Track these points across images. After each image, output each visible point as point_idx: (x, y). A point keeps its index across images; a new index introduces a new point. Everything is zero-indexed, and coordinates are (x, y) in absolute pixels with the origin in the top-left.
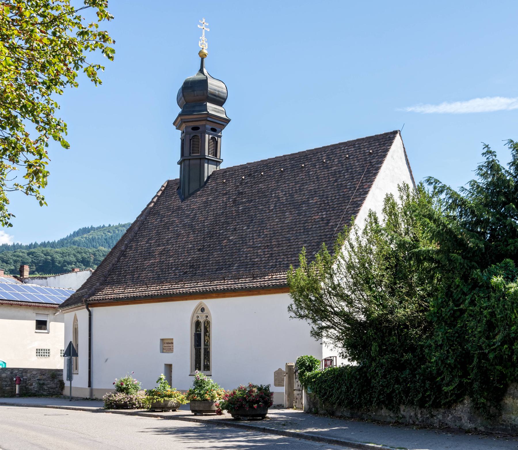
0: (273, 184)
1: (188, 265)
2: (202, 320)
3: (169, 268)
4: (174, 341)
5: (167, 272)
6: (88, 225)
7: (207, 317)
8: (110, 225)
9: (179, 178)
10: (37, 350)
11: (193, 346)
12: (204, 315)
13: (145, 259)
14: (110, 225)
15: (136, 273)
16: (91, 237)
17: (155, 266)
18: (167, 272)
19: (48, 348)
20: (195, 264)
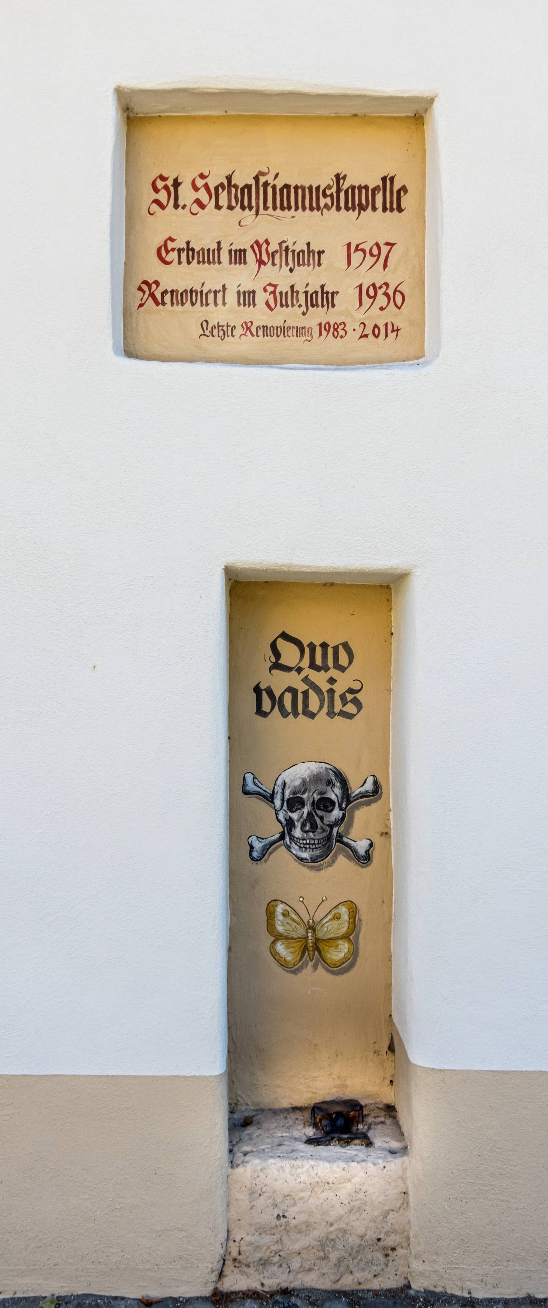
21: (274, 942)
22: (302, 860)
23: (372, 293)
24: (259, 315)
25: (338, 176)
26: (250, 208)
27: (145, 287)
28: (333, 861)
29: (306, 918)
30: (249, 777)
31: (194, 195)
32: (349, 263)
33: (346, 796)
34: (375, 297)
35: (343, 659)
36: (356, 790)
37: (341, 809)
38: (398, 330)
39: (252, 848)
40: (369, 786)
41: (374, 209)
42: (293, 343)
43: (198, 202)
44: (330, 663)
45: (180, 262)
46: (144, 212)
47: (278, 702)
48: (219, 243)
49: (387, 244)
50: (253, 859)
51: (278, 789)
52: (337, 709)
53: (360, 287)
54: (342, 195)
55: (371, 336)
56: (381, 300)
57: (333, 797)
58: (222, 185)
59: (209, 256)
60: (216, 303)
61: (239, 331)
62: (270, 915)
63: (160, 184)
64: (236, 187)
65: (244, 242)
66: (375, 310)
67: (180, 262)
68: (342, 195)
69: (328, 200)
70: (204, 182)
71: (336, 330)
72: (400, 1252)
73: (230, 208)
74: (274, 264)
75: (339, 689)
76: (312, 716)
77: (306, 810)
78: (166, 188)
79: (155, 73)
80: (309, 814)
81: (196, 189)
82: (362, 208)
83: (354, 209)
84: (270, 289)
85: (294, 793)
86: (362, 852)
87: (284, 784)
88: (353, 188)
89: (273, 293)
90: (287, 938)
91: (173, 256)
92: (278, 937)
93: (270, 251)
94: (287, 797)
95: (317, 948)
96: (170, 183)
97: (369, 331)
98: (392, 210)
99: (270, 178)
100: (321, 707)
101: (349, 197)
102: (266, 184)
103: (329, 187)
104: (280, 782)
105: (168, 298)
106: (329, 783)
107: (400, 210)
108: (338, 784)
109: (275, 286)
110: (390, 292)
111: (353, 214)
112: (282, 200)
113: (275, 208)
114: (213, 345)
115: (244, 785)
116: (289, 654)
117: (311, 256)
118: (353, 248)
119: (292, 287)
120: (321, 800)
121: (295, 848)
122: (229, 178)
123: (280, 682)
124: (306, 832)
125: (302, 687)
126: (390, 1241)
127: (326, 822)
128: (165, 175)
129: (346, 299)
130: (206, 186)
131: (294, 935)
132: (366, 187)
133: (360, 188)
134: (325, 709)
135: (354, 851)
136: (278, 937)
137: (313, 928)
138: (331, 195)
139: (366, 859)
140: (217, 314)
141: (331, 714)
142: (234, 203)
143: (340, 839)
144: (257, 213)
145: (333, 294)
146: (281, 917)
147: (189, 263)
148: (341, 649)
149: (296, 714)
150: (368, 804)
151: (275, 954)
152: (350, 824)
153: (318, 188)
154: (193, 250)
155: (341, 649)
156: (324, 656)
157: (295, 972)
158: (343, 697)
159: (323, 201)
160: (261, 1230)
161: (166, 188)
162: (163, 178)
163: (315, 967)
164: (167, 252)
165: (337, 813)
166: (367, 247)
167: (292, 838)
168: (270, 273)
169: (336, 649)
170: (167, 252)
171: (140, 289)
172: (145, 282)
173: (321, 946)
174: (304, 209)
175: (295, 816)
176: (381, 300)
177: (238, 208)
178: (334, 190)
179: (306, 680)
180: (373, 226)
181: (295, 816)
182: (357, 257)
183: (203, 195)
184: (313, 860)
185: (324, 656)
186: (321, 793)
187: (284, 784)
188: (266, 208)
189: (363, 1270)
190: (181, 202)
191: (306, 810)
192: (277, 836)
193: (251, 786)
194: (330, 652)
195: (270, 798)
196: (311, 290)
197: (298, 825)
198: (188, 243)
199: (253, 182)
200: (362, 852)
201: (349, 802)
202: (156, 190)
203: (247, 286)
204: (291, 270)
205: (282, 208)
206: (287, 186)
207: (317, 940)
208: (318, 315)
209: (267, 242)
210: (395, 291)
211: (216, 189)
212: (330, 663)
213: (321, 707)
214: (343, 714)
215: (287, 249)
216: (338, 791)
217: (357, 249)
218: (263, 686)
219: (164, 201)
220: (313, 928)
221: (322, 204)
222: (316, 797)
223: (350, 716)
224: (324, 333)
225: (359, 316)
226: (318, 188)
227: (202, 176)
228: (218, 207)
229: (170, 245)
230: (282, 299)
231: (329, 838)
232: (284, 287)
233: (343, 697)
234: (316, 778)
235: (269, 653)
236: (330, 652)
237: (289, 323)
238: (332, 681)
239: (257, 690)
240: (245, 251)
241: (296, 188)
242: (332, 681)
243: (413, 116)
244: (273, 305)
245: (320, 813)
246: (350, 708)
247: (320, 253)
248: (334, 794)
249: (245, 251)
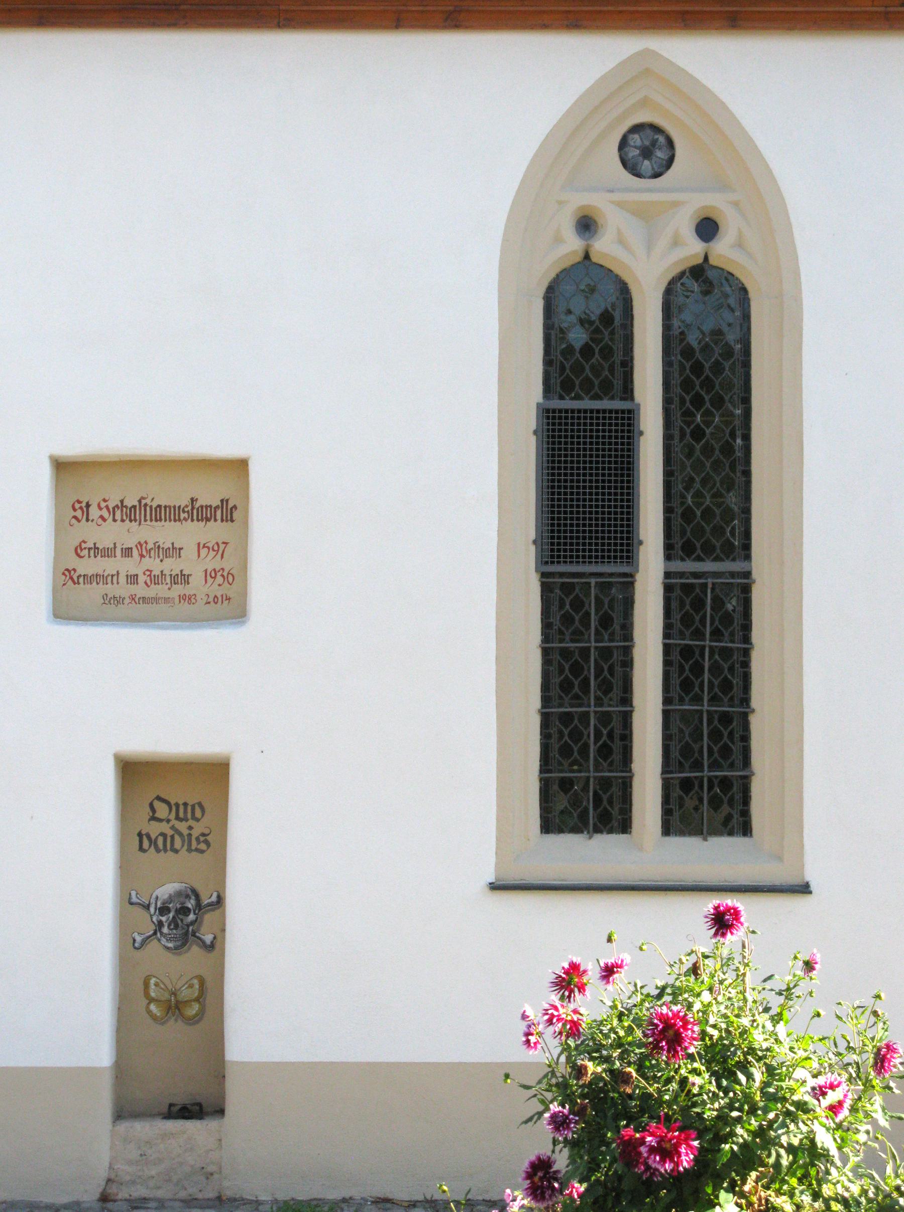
2: (647, 266)
7: (707, 228)
12: (682, 193)
21: (149, 1004)
22: (168, 948)
23: (213, 575)
24: (140, 590)
25: (192, 500)
26: (135, 520)
27: (67, 573)
28: (189, 949)
29: (170, 987)
30: (133, 893)
31: (99, 513)
32: (199, 556)
33: (199, 905)
34: (215, 577)
35: (198, 813)
36: (205, 901)
37: (195, 914)
38: (229, 599)
39: (134, 940)
40: (214, 898)
41: (216, 520)
42: (163, 607)
43: (102, 517)
44: (189, 815)
45: (89, 557)
46: (67, 524)
47: (153, 842)
48: (115, 544)
49: (224, 543)
50: (135, 948)
51: (153, 901)
52: (194, 847)
53: (206, 571)
54: (195, 512)
55: (212, 603)
56: (219, 579)
57: (190, 906)
58: (117, 506)
59: (108, 553)
60: (112, 583)
61: (127, 601)
62: (146, 984)
63: (77, 506)
64: (126, 507)
65: (131, 543)
66: (215, 586)
67: (89, 557)
68: (195, 512)
69: (186, 515)
70: (106, 504)
71: (190, 599)
72: (216, 1176)
73: (123, 521)
74: (150, 557)
75: (195, 833)
76: (176, 851)
77: (171, 915)
78: (81, 508)
79: (71, 449)
80: (174, 917)
81: (100, 508)
82: (208, 520)
83: (202, 520)
84: (148, 573)
85: (163, 904)
86: (208, 942)
87: (157, 898)
88: (202, 507)
89: (150, 575)
90: (156, 1000)
91: (85, 552)
92: (151, 1000)
93: (149, 548)
94: (158, 906)
95: (177, 1007)
96: (84, 505)
97: (211, 599)
98: (227, 521)
99: (148, 501)
100: (183, 846)
101: (201, 513)
102: (146, 505)
103: (187, 506)
104: (154, 896)
105: (81, 580)
106: (188, 896)
107: (232, 521)
108: (193, 897)
109: (151, 571)
110: (225, 574)
111: (202, 524)
112: (156, 515)
113: (151, 520)
114: (111, 609)
115: (130, 898)
116: (162, 811)
117: (175, 551)
118: (201, 546)
119: (162, 572)
120: (181, 908)
121: (164, 941)
122: (122, 501)
123: (155, 829)
124: (171, 930)
125: (170, 832)
126: (211, 1168)
127: (185, 922)
128: (81, 500)
129: (197, 580)
130: (107, 507)
131: (163, 999)
132: (211, 506)
133: (207, 507)
134: (186, 847)
135: (203, 942)
136: (151, 1000)
137: (174, 994)
138: (188, 512)
139: (211, 947)
140: (110, 589)
141: (189, 850)
142: (125, 518)
143: (194, 934)
144: (140, 524)
145: (188, 576)
146: (153, 987)
147: (95, 557)
148: (197, 806)
149: (165, 850)
150: (213, 910)
151: (149, 1012)
152: (201, 923)
153: (179, 507)
154: (98, 548)
155: (197, 806)
156: (185, 812)
157: (162, 1024)
158: (197, 839)
159: (183, 516)
160: (130, 1163)
161: (81, 508)
162: (79, 502)
163: (176, 1020)
164: (82, 550)
165: (192, 917)
166: (210, 545)
167: (162, 933)
168: (148, 563)
169: (193, 807)
170: (82, 550)
171: (64, 574)
172: (67, 570)
173: (180, 1006)
174: (170, 520)
175: (164, 919)
176: (219, 579)
177: (127, 521)
178: (190, 508)
179: (173, 828)
180: (215, 531)
181: (164, 919)
182: (204, 552)
183: (105, 513)
184: (176, 948)
185: (185, 812)
186: (182, 903)
187: (157, 898)
188: (146, 520)
189: (193, 1187)
190: (91, 518)
191: (171, 915)
192: (151, 932)
193: (134, 899)
194: (189, 808)
195: (147, 907)
196: (174, 573)
197: (166, 925)
198: (95, 544)
199: (137, 503)
200: (208, 942)
201: (200, 910)
202: (75, 510)
203: (133, 572)
204: (161, 561)
205: (156, 520)
206: (159, 506)
207: (177, 1002)
208: (178, 589)
209: (146, 543)
210: (228, 573)
211: (114, 509)
212: (189, 815)
213: (183, 846)
214: (197, 850)
215: (159, 547)
216: (193, 902)
217: (204, 547)
218: (144, 832)
219: (80, 517)
220: (174, 994)
221: (182, 518)
222: (178, 906)
223: (202, 852)
224: (182, 601)
225: (205, 590)
226: (179, 507)
227: (105, 501)
228: (115, 520)
229: (83, 546)
230: (155, 579)
231: (186, 933)
232: (156, 572)
233: (197, 839)
234: (179, 894)
235: (148, 809)
236: (189, 808)
237: (160, 595)
238: (190, 828)
239: (140, 835)
240: (131, 548)
241: (165, 507)
242: (190, 828)
243: (240, 466)
244: (149, 583)
245: (181, 917)
246: (203, 846)
247: (180, 549)
248: (191, 903)
249: (131, 548)
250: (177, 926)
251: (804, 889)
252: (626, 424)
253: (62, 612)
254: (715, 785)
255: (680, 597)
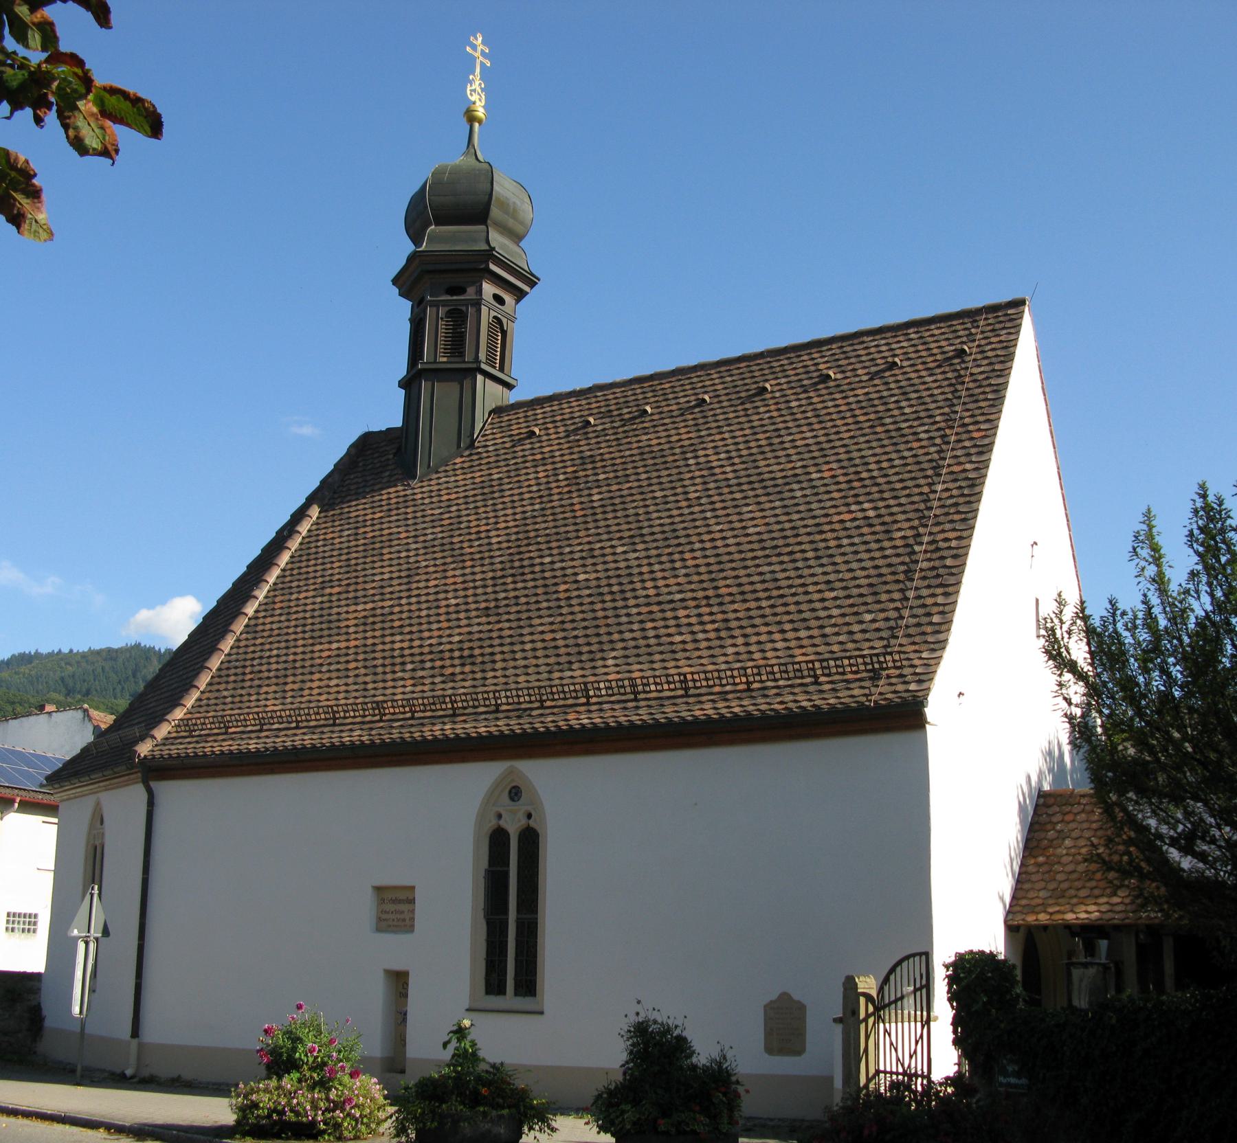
0: (686, 435)
1: (457, 654)
2: (513, 829)
3: (393, 665)
4: (418, 895)
5: (389, 677)
6: (30, 648)
7: (529, 816)
8: (71, 651)
9: (398, 423)
10: (9, 915)
11: (481, 914)
12: (522, 807)
13: (316, 639)
14: (71, 651)
15: (290, 679)
16: (33, 673)
17: (351, 658)
18: (389, 677)
19: (34, 912)
20: (477, 652)
79: (378, 884)
117: (402, 912)
243: (413, 888)
250: (399, 1018)
251: (542, 1013)
252: (506, 874)
253: (379, 929)
254: (528, 985)
255: (520, 925)
